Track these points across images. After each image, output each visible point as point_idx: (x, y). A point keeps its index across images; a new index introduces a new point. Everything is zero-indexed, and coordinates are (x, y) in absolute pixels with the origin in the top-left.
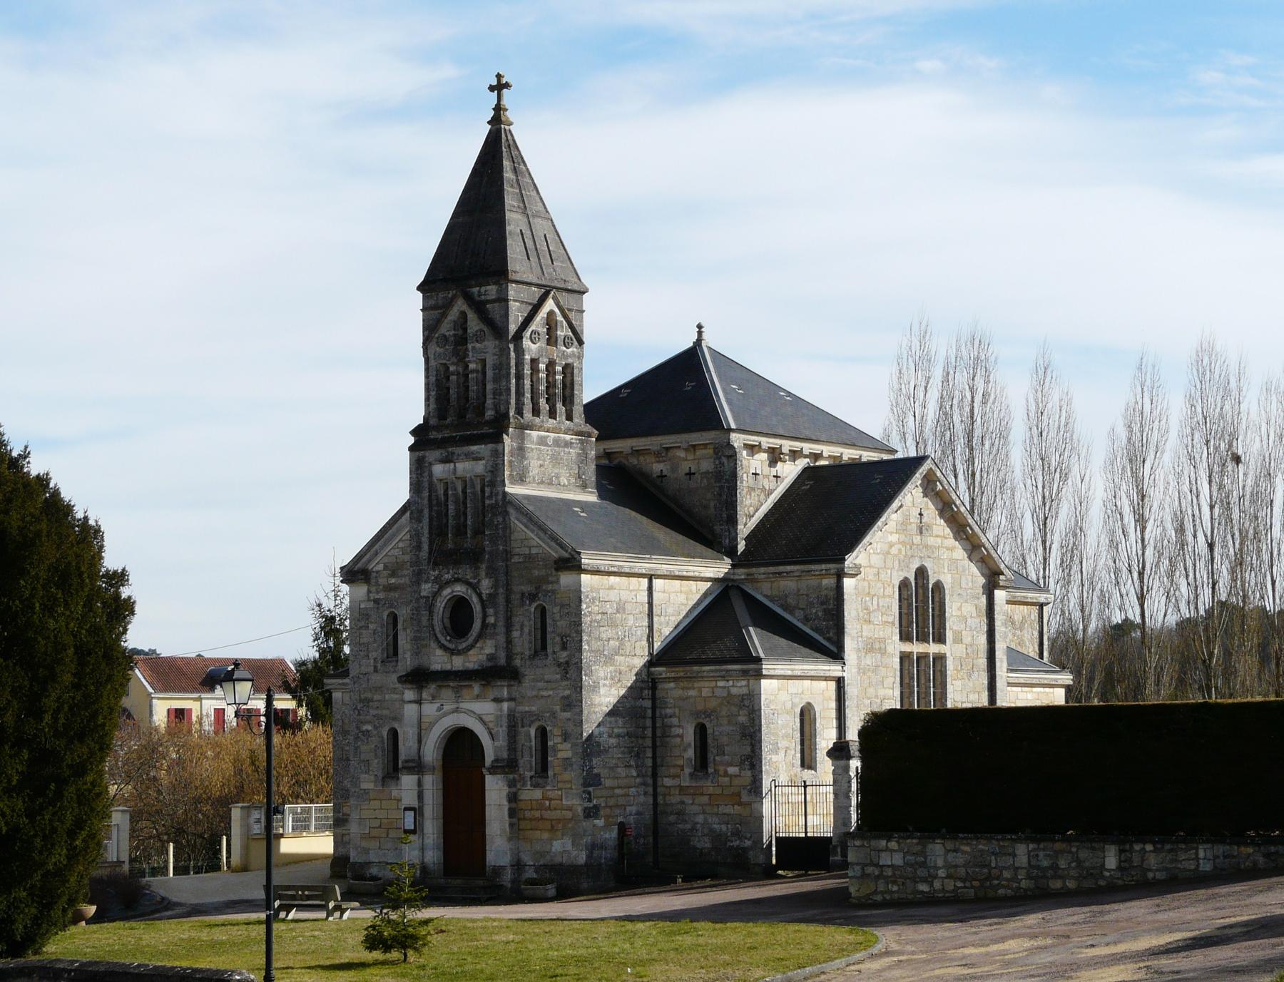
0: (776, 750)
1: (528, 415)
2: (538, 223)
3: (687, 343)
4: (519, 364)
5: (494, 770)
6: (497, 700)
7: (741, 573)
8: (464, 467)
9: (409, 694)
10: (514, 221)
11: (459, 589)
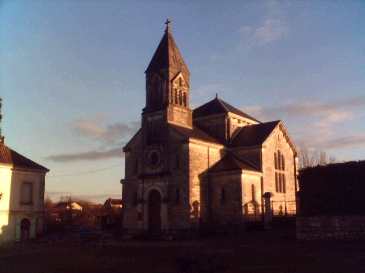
0: (246, 196)
1: (174, 103)
2: (178, 55)
3: (212, 98)
4: (172, 89)
5: (163, 202)
6: (165, 181)
7: (232, 150)
8: (156, 118)
9: (140, 181)
10: (171, 53)
11: (155, 151)
